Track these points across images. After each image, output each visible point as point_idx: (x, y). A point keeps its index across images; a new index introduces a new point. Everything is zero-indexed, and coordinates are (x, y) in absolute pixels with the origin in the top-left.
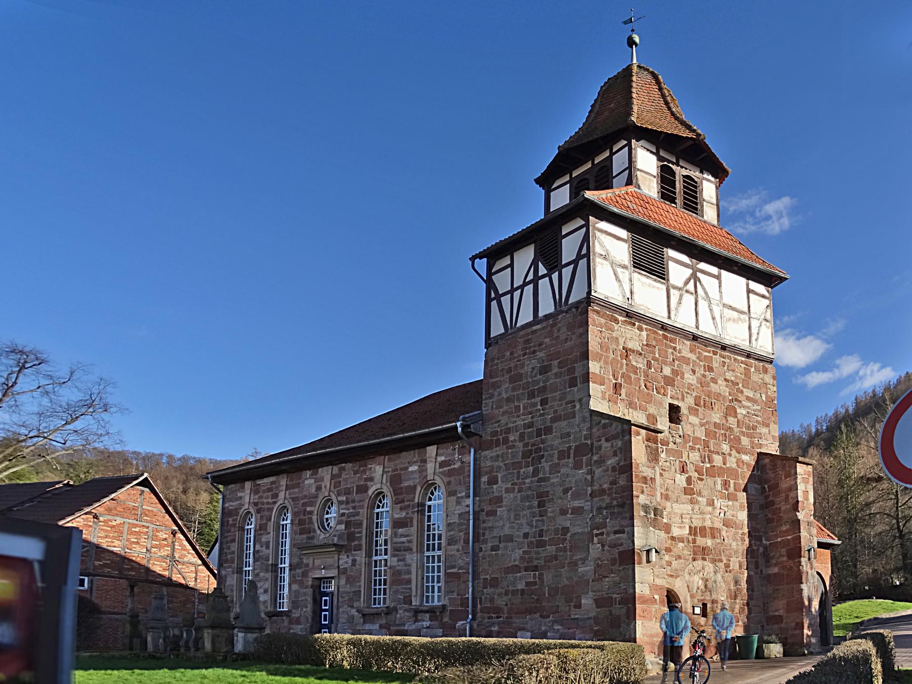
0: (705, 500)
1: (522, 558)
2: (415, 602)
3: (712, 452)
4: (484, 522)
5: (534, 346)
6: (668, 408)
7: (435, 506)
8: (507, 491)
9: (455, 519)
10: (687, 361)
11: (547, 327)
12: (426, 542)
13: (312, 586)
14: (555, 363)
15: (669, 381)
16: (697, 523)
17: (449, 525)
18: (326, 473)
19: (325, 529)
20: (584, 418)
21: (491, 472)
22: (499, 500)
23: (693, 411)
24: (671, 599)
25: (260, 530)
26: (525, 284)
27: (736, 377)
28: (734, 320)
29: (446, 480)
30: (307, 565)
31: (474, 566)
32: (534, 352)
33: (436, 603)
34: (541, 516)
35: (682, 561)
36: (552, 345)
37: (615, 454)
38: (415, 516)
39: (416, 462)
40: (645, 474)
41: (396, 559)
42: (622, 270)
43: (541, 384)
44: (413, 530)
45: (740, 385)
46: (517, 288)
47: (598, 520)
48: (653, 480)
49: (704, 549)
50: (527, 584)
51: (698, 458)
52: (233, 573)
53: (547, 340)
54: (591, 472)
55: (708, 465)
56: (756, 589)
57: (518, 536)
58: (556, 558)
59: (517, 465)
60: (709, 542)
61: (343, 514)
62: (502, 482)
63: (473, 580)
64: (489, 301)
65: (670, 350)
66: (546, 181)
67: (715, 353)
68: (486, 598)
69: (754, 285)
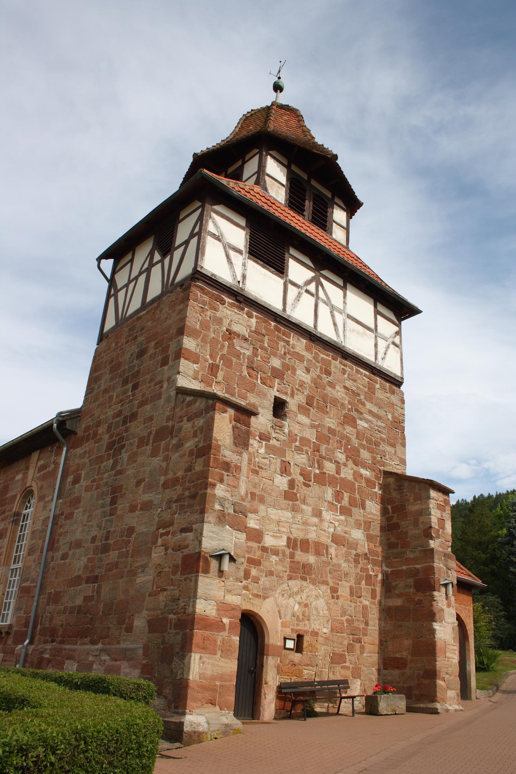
0: (310, 509)
1: (86, 567)
3: (324, 458)
4: (61, 527)
5: (137, 332)
6: (273, 400)
10: (300, 358)
11: (152, 309)
14: (153, 344)
15: (277, 374)
16: (297, 534)
20: (168, 400)
21: (77, 470)
22: (78, 500)
23: (303, 409)
24: (251, 625)
26: (140, 274)
27: (358, 388)
28: (358, 333)
29: (40, 484)
31: (43, 578)
32: (136, 337)
35: (275, 578)
37: (195, 435)
40: (227, 459)
43: (136, 369)
45: (362, 397)
47: (167, 516)
48: (238, 468)
49: (304, 566)
50: (86, 599)
51: (305, 461)
53: (149, 324)
54: (167, 459)
55: (317, 471)
56: (370, 623)
58: (116, 565)
59: (100, 460)
60: (312, 559)
62: (84, 480)
63: (40, 595)
68: (46, 616)
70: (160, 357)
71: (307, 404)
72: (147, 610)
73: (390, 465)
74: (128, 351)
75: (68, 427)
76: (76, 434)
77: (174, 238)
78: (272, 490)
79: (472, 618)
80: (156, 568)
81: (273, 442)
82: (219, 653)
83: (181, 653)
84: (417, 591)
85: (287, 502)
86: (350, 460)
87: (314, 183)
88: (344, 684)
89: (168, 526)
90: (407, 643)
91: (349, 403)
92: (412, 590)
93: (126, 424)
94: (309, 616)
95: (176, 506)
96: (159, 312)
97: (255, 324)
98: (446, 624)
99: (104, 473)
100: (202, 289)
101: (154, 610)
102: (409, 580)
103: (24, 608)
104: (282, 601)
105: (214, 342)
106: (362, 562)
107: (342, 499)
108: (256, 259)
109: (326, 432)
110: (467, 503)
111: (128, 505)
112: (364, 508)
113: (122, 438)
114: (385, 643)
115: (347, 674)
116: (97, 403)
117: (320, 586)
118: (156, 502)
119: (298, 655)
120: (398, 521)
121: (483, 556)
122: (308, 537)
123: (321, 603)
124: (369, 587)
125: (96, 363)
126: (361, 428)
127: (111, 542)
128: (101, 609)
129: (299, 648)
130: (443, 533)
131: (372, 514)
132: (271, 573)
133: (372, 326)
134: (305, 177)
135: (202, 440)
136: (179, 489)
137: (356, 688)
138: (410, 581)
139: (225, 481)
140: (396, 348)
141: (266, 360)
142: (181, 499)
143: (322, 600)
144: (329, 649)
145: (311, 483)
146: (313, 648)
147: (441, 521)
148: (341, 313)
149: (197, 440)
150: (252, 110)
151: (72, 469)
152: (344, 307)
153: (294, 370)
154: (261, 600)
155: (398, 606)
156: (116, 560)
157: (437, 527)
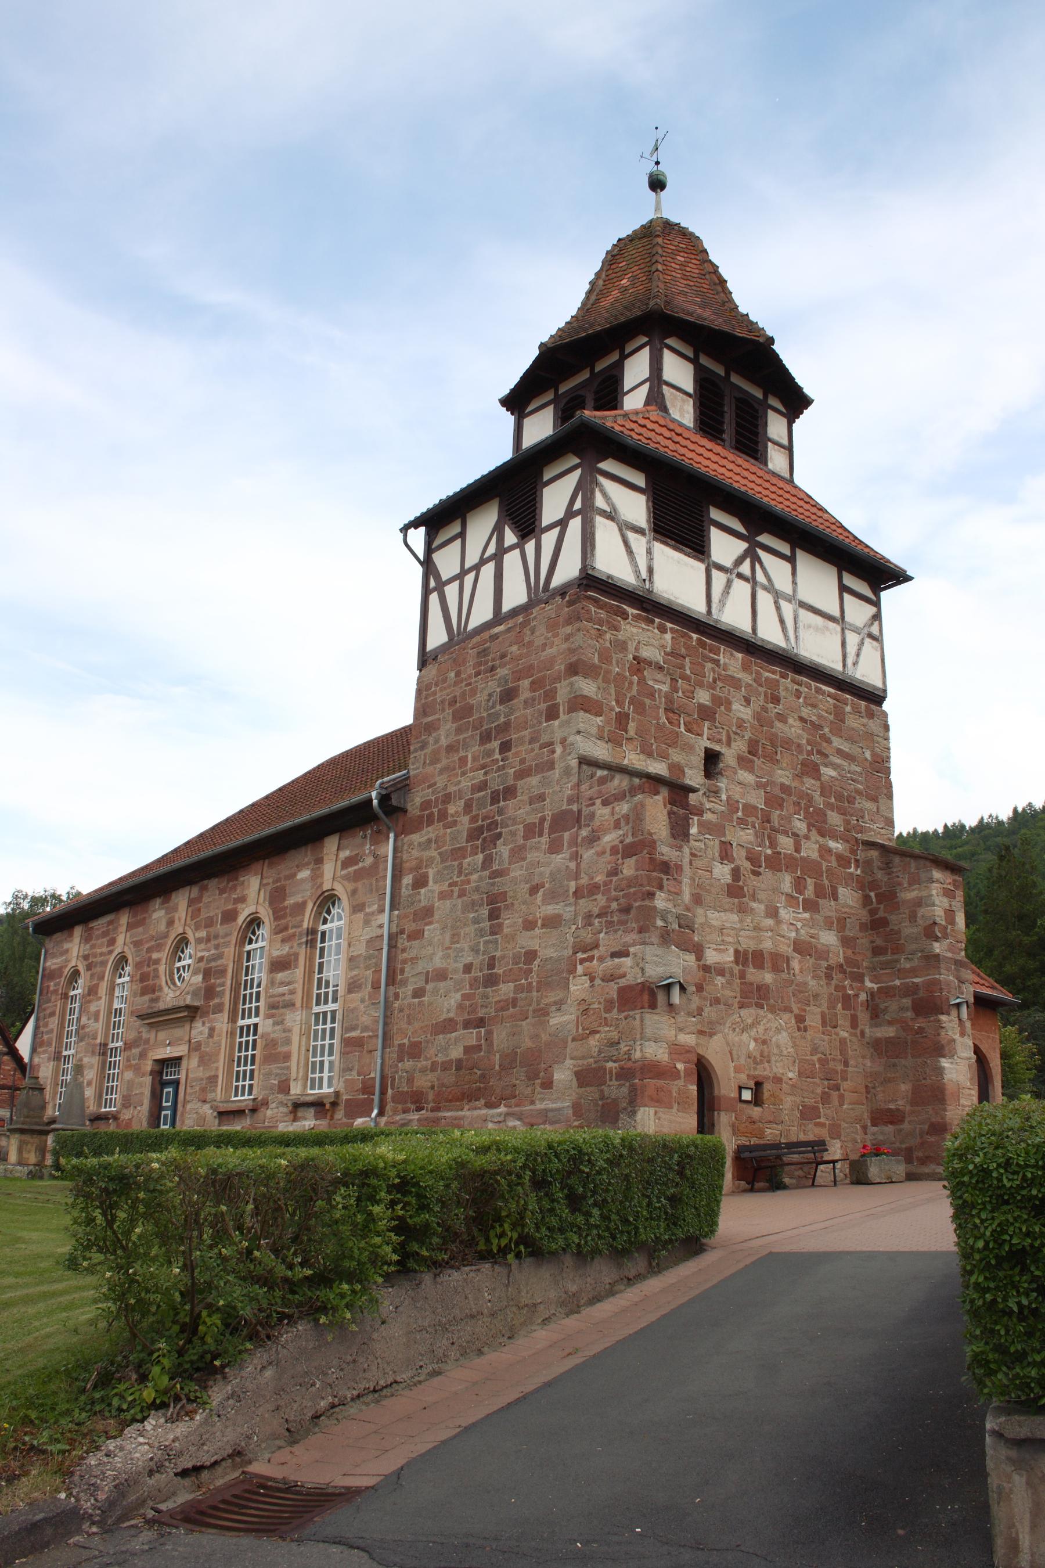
0: (762, 907)
1: (460, 1007)
2: (296, 1089)
4: (404, 950)
5: (494, 660)
6: (703, 755)
7: (331, 931)
8: (443, 896)
9: (361, 949)
10: (736, 683)
11: (515, 626)
12: (316, 991)
13: (152, 1073)
14: (526, 683)
15: (707, 714)
16: (747, 944)
17: (351, 959)
18: (181, 899)
19: (174, 984)
20: (567, 771)
21: (418, 867)
23: (744, 762)
25: (89, 994)
26: (483, 561)
27: (820, 717)
28: (817, 629)
29: (350, 886)
30: (147, 1041)
31: (385, 1024)
32: (493, 669)
33: (326, 1090)
34: (493, 933)
35: (722, 1007)
36: (520, 657)
37: (617, 825)
38: (302, 952)
39: (308, 864)
40: (666, 858)
41: (271, 1021)
42: (636, 535)
44: (299, 973)
45: (827, 730)
46: (470, 570)
47: (586, 935)
48: (679, 868)
49: (759, 988)
50: (467, 1050)
51: (751, 838)
52: (49, 1059)
53: (514, 648)
54: (576, 857)
55: (769, 851)
56: (852, 1062)
57: (455, 971)
58: (514, 1002)
59: (458, 853)
60: (768, 977)
61: (201, 959)
62: (435, 882)
63: (384, 1047)
64: (426, 592)
65: (709, 665)
66: (518, 401)
67: (784, 676)
68: (400, 1078)
69: (849, 581)
70: (543, 706)
71: (749, 752)
72: (572, 1059)
73: (871, 830)
74: (483, 689)
75: (394, 802)
76: (406, 811)
77: (537, 511)
78: (711, 885)
79: (998, 1051)
80: (579, 1004)
81: (708, 816)
82: (676, 1106)
83: (630, 1109)
84: (917, 1015)
85: (731, 900)
86: (814, 829)
87: (735, 379)
88: (819, 1145)
89: (591, 950)
90: (905, 1088)
91: (809, 743)
92: (909, 1014)
93: (499, 802)
94: (769, 1056)
95: (600, 922)
96: (528, 632)
97: (670, 642)
98: (959, 1060)
99: (471, 874)
100: (596, 601)
101: (583, 1058)
102: (904, 1000)
103: (356, 1067)
104: (734, 1038)
105: (620, 678)
106: (837, 976)
107: (805, 888)
108: (664, 539)
109: (777, 791)
110: (1000, 823)
111: (520, 920)
112: (836, 899)
113: (495, 824)
114: (872, 1090)
115: (823, 1133)
116: (439, 766)
117: (782, 1014)
118: (567, 916)
119: (758, 1109)
120: (886, 915)
121: (1026, 940)
122: (761, 946)
123: (783, 1038)
124: (848, 1012)
125: (423, 701)
126: (827, 778)
127: (498, 970)
128: (497, 1062)
129: (757, 1101)
130: (953, 931)
131: (847, 906)
132: (717, 1001)
133: (836, 613)
134: (720, 371)
135: (630, 834)
136: (601, 899)
137: (835, 1150)
138: (907, 1002)
139: (665, 888)
140: (875, 643)
141: (690, 695)
142: (606, 913)
143: (784, 1034)
144: (798, 1100)
145: (761, 870)
146: (777, 1100)
147: (950, 914)
148: (790, 601)
149: (621, 832)
150: (620, 240)
151: (407, 865)
152: (795, 591)
153: (729, 703)
154: (706, 1038)
155: (890, 1038)
156: (512, 995)
157: (943, 923)
